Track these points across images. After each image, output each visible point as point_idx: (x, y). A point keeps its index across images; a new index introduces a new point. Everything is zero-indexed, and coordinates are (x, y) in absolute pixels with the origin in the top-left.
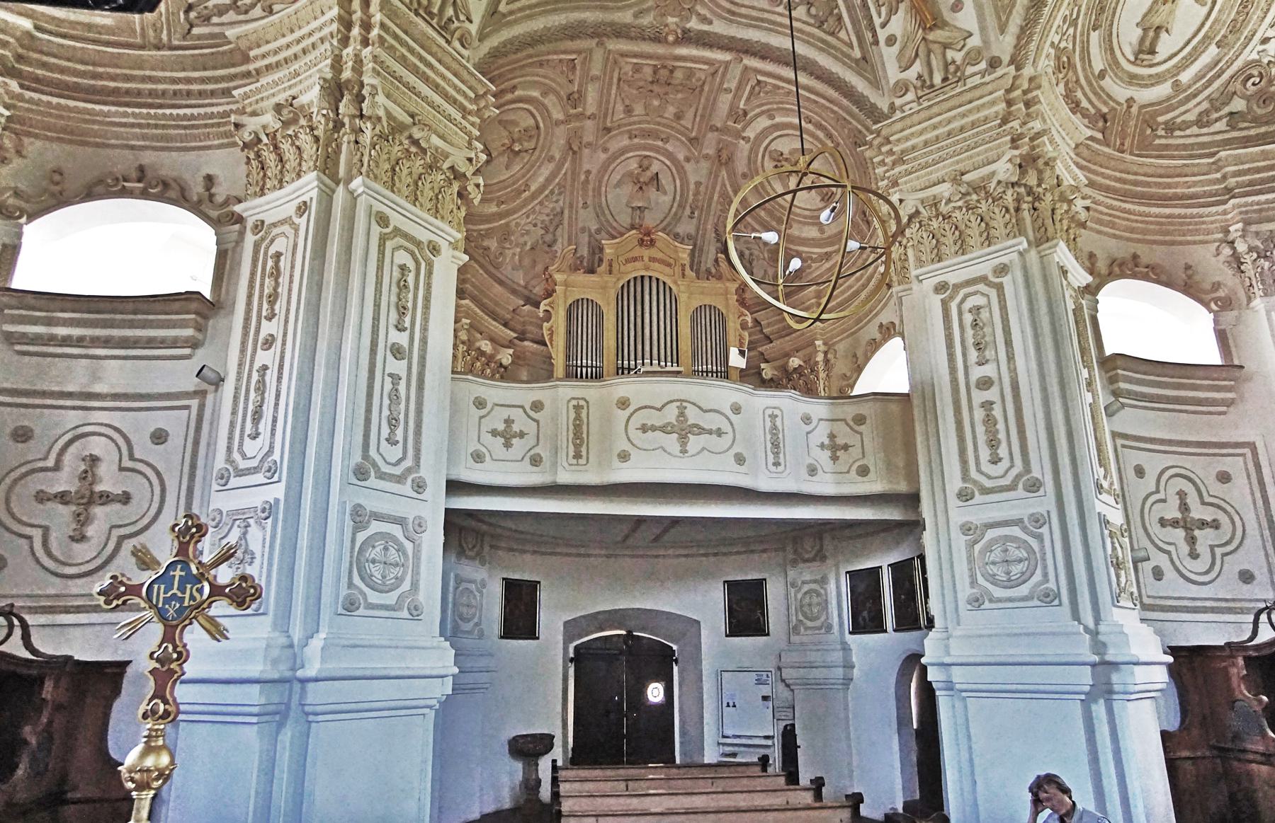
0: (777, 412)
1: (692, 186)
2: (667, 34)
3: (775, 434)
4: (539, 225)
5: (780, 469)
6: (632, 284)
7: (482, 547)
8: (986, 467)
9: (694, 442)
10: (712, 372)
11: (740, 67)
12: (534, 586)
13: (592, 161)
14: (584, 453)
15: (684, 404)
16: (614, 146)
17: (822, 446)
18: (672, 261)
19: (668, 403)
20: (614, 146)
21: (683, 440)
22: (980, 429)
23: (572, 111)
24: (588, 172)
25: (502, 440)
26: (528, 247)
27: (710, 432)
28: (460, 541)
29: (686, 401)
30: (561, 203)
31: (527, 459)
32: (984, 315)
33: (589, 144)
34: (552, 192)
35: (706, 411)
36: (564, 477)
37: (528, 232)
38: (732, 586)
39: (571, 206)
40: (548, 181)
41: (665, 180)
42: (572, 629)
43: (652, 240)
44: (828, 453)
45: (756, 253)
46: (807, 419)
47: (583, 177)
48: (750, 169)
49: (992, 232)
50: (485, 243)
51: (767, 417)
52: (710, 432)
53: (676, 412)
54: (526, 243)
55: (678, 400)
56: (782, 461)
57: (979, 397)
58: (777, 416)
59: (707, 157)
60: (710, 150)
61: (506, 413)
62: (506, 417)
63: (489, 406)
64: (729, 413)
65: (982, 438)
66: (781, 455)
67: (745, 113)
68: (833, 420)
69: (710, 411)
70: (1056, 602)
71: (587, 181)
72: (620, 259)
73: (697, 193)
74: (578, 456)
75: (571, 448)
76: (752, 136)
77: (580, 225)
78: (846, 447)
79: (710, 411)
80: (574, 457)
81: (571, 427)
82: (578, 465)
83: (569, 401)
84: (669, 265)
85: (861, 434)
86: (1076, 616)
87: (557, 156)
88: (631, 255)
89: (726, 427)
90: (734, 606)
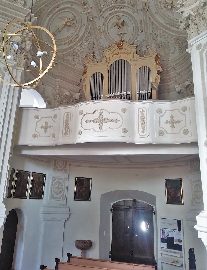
1: (139, 22)
3: (143, 119)
4: (86, 48)
5: (145, 133)
6: (115, 63)
9: (105, 125)
10: (99, 97)
12: (89, 180)
13: (99, 23)
14: (68, 132)
15: (102, 111)
16: (105, 15)
17: (167, 122)
18: (130, 52)
19: (96, 111)
20: (105, 15)
21: (101, 125)
23: (85, 7)
24: (99, 26)
25: (44, 129)
26: (84, 57)
27: (112, 121)
28: (55, 164)
30: (92, 39)
31: (51, 136)
33: (96, 17)
35: (110, 113)
36: (61, 141)
37: (83, 52)
38: (169, 181)
39: (96, 39)
40: (158, 22)
41: (127, 22)
42: (105, 197)
43: (121, 45)
44: (170, 125)
45: (169, 41)
46: (160, 111)
47: (98, 28)
50: (67, 58)
52: (112, 121)
53: (99, 114)
56: (145, 130)
59: (140, 10)
61: (45, 120)
62: (46, 121)
64: (121, 113)
66: (145, 128)
68: (171, 110)
69: (112, 112)
73: (141, 23)
74: (66, 134)
78: (178, 122)
79: (112, 112)
81: (65, 123)
82: (66, 137)
83: (65, 113)
85: (185, 115)
87: (86, 23)
88: (115, 52)
89: (119, 118)
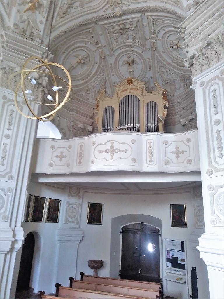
0: (151, 141)
2: (117, 14)
7: (79, 192)
8: (218, 159)
9: (116, 155)
11: (146, 17)
12: (100, 205)
13: (111, 61)
15: (113, 142)
16: (117, 53)
17: (173, 152)
18: (138, 88)
20: (117, 53)
22: (216, 142)
23: (97, 46)
26: (97, 92)
27: (122, 151)
29: (114, 141)
32: (217, 93)
33: (108, 55)
34: (100, 73)
38: (174, 206)
39: (108, 75)
44: (175, 155)
45: (175, 79)
48: (164, 50)
49: (220, 56)
50: (81, 93)
51: (147, 143)
52: (122, 151)
54: (95, 91)
55: (111, 141)
57: (215, 128)
58: (152, 142)
59: (149, 49)
60: (148, 47)
63: (56, 148)
64: (131, 144)
65: (216, 146)
66: (153, 157)
67: (155, 31)
70: (7, 221)
71: (111, 66)
72: (121, 91)
73: (149, 62)
74: (80, 163)
75: (78, 160)
76: (161, 38)
77: (113, 82)
78: (183, 152)
80: (79, 163)
81: (79, 153)
83: (79, 144)
84: (137, 89)
86: (10, 226)
87: (98, 61)
88: (125, 88)
90: (174, 214)
